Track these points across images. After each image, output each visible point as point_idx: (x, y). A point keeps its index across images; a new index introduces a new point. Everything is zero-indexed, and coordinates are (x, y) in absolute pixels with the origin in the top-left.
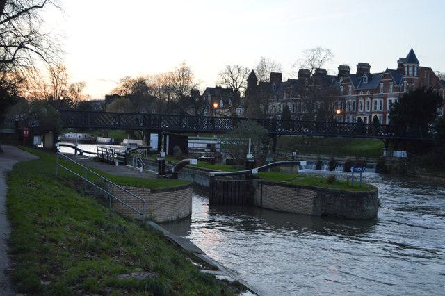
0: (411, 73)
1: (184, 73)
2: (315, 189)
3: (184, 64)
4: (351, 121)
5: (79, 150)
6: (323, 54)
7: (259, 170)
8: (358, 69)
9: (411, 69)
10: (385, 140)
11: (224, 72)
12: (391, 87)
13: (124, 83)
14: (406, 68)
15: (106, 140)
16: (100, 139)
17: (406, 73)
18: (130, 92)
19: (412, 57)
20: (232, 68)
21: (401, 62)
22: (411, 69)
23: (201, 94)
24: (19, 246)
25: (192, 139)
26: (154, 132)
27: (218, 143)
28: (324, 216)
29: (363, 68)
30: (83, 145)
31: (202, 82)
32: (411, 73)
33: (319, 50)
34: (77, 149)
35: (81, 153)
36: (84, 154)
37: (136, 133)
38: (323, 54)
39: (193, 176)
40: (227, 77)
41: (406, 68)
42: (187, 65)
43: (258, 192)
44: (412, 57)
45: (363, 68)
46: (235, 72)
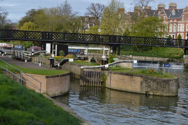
1: (67, 8)
3: (66, 2)
7: (109, 65)
10: (184, 49)
11: (90, 7)
26: (48, 42)
28: (147, 95)
40: (92, 10)
42: (69, 2)
43: (108, 78)
46: (97, 7)
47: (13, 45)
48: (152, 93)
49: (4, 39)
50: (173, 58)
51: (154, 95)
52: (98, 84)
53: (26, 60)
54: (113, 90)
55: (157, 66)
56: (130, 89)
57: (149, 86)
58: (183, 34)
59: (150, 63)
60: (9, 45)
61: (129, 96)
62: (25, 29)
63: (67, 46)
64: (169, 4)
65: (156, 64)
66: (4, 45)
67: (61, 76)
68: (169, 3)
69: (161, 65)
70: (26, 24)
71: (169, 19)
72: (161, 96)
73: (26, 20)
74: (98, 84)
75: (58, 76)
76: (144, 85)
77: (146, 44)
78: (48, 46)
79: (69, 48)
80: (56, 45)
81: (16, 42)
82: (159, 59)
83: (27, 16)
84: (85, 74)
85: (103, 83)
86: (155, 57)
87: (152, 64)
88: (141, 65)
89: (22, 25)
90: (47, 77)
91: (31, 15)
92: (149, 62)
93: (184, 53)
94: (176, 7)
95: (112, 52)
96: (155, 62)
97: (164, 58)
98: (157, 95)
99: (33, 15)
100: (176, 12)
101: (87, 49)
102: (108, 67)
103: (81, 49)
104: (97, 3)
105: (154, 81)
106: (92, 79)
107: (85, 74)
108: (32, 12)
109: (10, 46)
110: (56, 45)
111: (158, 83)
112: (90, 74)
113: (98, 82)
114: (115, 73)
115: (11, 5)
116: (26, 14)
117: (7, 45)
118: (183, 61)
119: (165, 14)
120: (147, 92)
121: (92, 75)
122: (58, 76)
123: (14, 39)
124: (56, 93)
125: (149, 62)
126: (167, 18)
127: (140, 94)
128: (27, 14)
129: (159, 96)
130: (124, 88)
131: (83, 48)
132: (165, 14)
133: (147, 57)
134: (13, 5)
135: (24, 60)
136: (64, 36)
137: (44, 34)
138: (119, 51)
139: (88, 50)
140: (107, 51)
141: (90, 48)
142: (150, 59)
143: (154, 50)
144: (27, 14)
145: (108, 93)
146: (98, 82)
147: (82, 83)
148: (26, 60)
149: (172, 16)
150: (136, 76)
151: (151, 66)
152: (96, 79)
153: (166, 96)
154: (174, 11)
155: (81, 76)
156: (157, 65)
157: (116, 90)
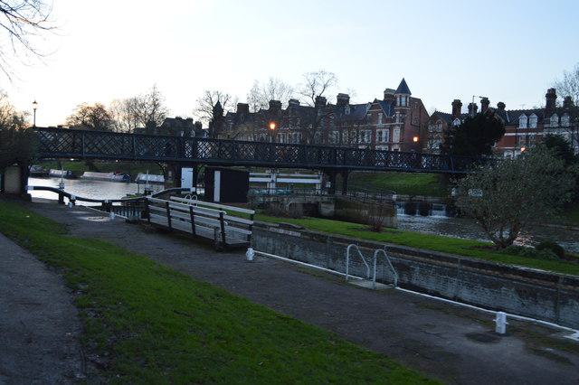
0: (403, 103)
4: (282, 141)
5: (69, 196)
8: (386, 96)
9: (403, 99)
12: (381, 117)
13: (80, 110)
14: (398, 99)
15: (60, 172)
16: (53, 172)
17: (398, 104)
18: (142, 126)
19: (404, 87)
20: (212, 93)
21: (388, 93)
22: (403, 99)
23: (205, 126)
24: (163, 342)
25: (254, 176)
27: (273, 182)
29: (343, 99)
30: (35, 179)
32: (403, 103)
33: (323, 73)
34: (62, 194)
35: (73, 201)
36: (78, 203)
37: (97, 163)
38: (326, 78)
39: (195, 193)
41: (398, 99)
44: (404, 87)
45: (343, 99)
78: (187, 174)
79: (251, 179)
80: (217, 175)
95: (328, 185)
110: (217, 175)
138: (345, 183)
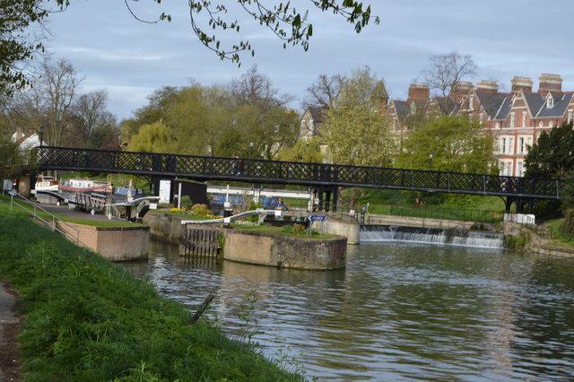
2: (272, 237)
3: (254, 71)
6: (460, 63)
7: (232, 220)
10: (505, 198)
20: (329, 80)
26: (166, 178)
28: (279, 267)
31: (292, 98)
38: (460, 63)
47: (111, 187)
48: (286, 265)
49: (91, 171)
50: (485, 222)
51: (290, 268)
52: (211, 252)
53: (93, 212)
54: (232, 261)
55: (440, 240)
56: (254, 258)
57: (283, 253)
58: (512, 161)
59: (425, 233)
60: (101, 185)
61: (253, 270)
62: (144, 142)
63: (205, 187)
64: (540, 79)
65: (437, 234)
66: (86, 187)
67: (124, 229)
68: (540, 76)
69: (448, 239)
70: (145, 130)
71: (535, 121)
72: (301, 269)
73: (148, 117)
74: (211, 252)
75: (119, 229)
76: (276, 250)
77: (329, 180)
78: (165, 186)
79: (209, 190)
80: (180, 184)
81: (121, 179)
82: (446, 224)
83: (288, 124)
84: (188, 234)
85: (220, 251)
86: (444, 218)
87: (428, 236)
88: (402, 238)
89: (137, 133)
90: (99, 229)
91: (162, 104)
92: (423, 230)
93: (504, 208)
94: (560, 86)
95: (317, 202)
96: (436, 231)
97: (465, 220)
98: (294, 269)
99: (169, 106)
100: (555, 101)
101: (257, 194)
102: (155, 208)
103: (277, 198)
104: (335, 73)
105: (292, 243)
106: (201, 244)
107: (188, 234)
108: (165, 94)
109: (102, 188)
110: (180, 184)
111: (296, 248)
112: (197, 235)
113: (211, 249)
114: (235, 232)
115: (149, 58)
116: (149, 101)
117: (96, 185)
118: (503, 229)
119: (526, 104)
120: (280, 263)
121: (200, 237)
122: (119, 229)
123: (115, 170)
124: (116, 256)
125: (423, 230)
126: (532, 117)
127: (269, 266)
128: (151, 99)
129: (297, 269)
130: (246, 258)
131: (251, 193)
132: (527, 106)
133: (426, 219)
134: (156, 57)
135: (89, 212)
136: (205, 164)
137: (156, 158)
139: (260, 197)
140: (308, 200)
141: (263, 193)
142: (435, 223)
143: (451, 203)
144: (151, 99)
145: (225, 264)
146: (211, 249)
147: (182, 250)
148: (93, 212)
149: (545, 112)
150: (265, 235)
151: (425, 240)
152: (208, 243)
153: (309, 270)
154: (551, 97)
155: (181, 238)
156: (439, 237)
157: (236, 262)
